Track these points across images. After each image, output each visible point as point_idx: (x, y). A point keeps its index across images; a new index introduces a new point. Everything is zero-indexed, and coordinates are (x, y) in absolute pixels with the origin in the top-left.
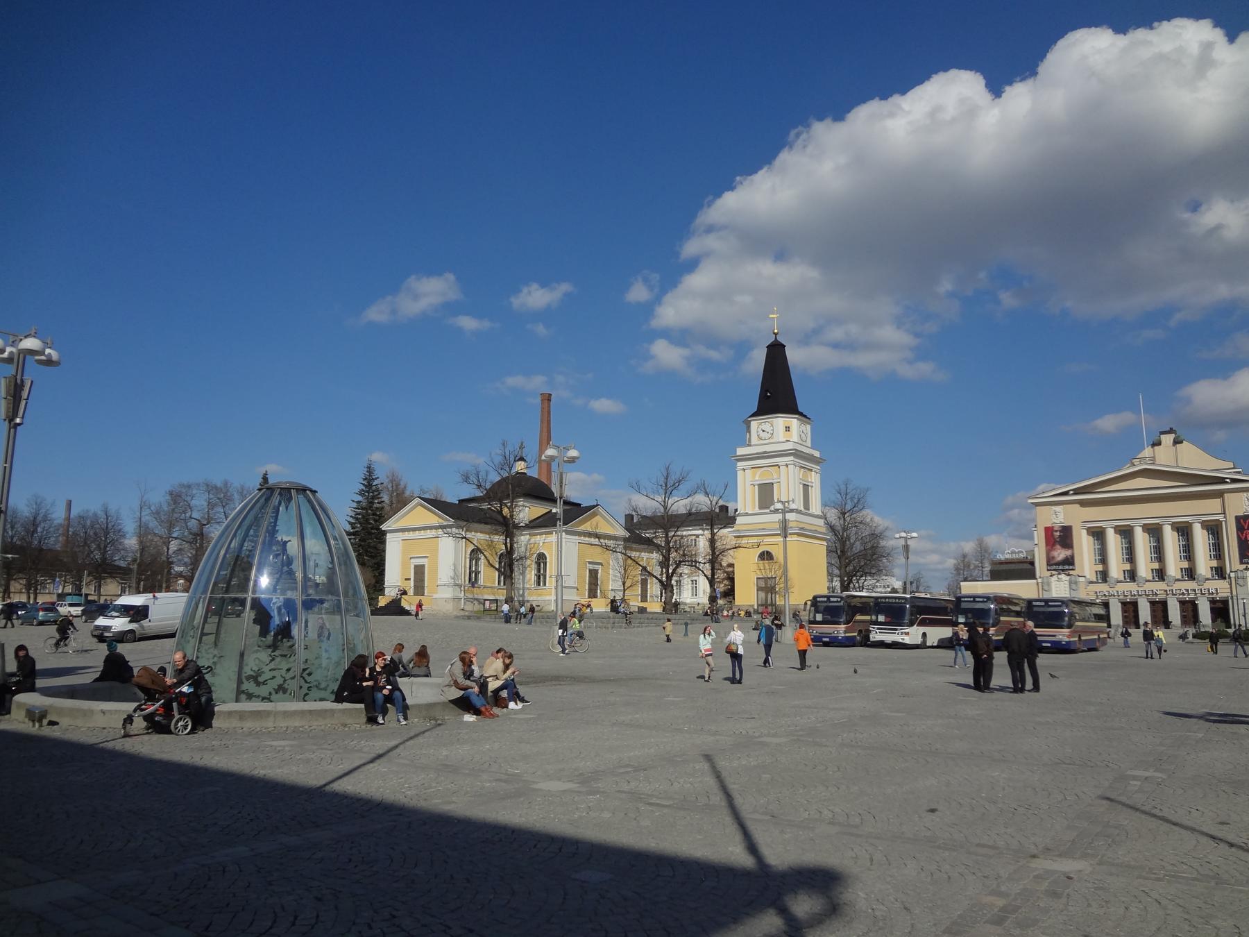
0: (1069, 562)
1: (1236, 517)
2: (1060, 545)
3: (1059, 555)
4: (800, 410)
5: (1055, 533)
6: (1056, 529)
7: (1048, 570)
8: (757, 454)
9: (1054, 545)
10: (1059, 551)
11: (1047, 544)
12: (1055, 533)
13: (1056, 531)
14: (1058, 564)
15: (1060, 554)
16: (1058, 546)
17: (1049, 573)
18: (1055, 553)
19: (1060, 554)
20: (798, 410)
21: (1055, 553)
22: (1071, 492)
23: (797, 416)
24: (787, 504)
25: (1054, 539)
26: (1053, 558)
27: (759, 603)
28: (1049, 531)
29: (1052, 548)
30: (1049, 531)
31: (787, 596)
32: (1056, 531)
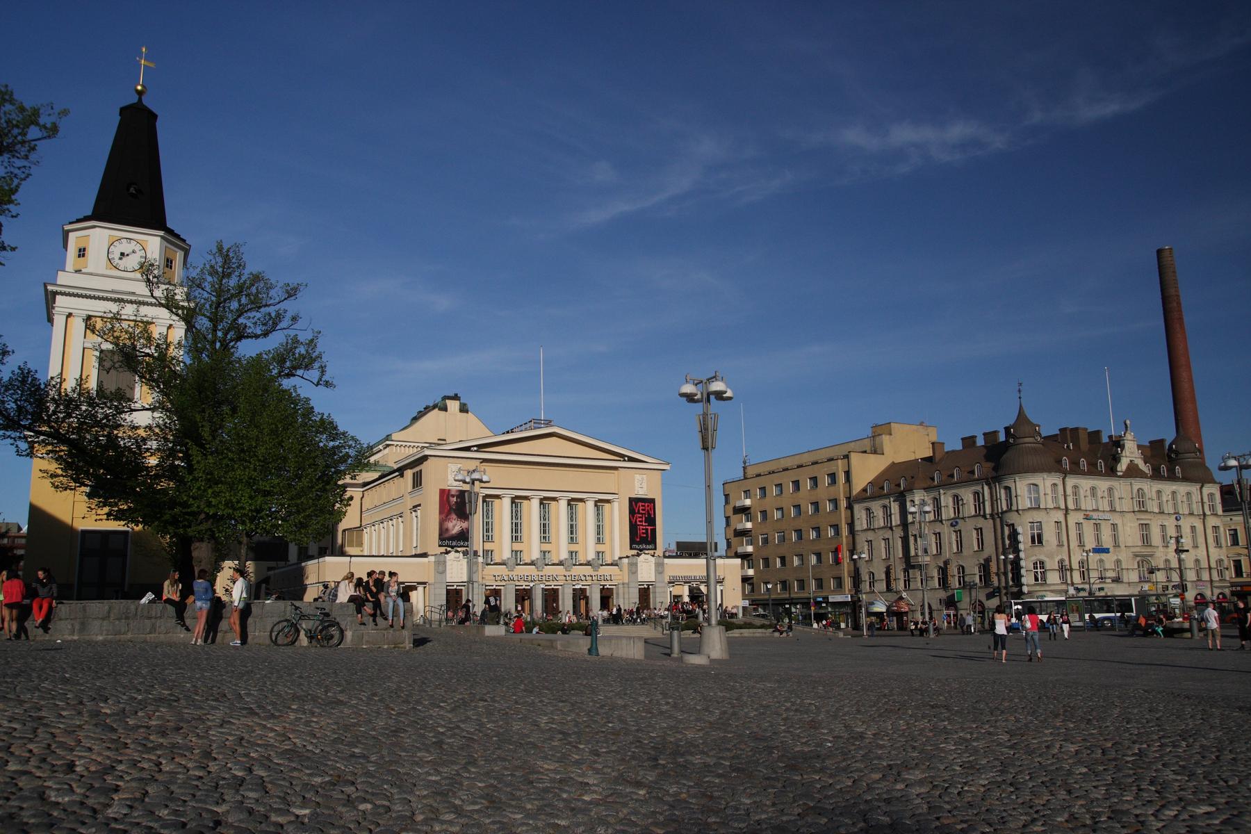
0: (464, 536)
1: (630, 498)
2: (456, 515)
3: (454, 527)
4: (169, 225)
5: (451, 499)
6: (453, 493)
7: (440, 546)
8: (112, 292)
9: (449, 514)
10: (454, 522)
11: (441, 513)
12: (451, 499)
13: (453, 496)
14: (453, 538)
15: (455, 526)
16: (454, 516)
17: (443, 549)
18: (450, 525)
19: (455, 526)
20: (166, 224)
21: (450, 525)
22: (475, 448)
23: (162, 233)
24: (1241, 460)
25: (450, 506)
26: (447, 530)
27: (1236, 632)
28: (445, 494)
29: (447, 516)
30: (445, 494)
31: (794, 601)
32: (453, 496)
